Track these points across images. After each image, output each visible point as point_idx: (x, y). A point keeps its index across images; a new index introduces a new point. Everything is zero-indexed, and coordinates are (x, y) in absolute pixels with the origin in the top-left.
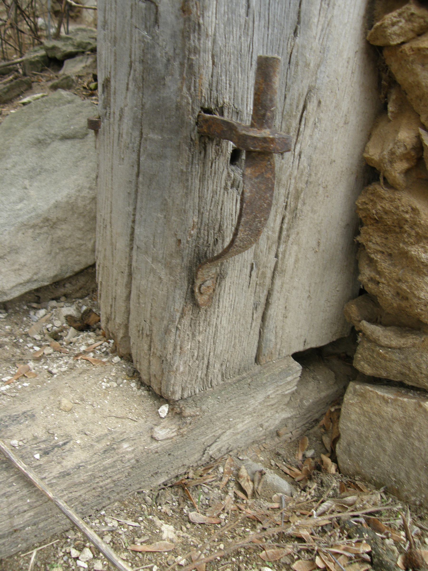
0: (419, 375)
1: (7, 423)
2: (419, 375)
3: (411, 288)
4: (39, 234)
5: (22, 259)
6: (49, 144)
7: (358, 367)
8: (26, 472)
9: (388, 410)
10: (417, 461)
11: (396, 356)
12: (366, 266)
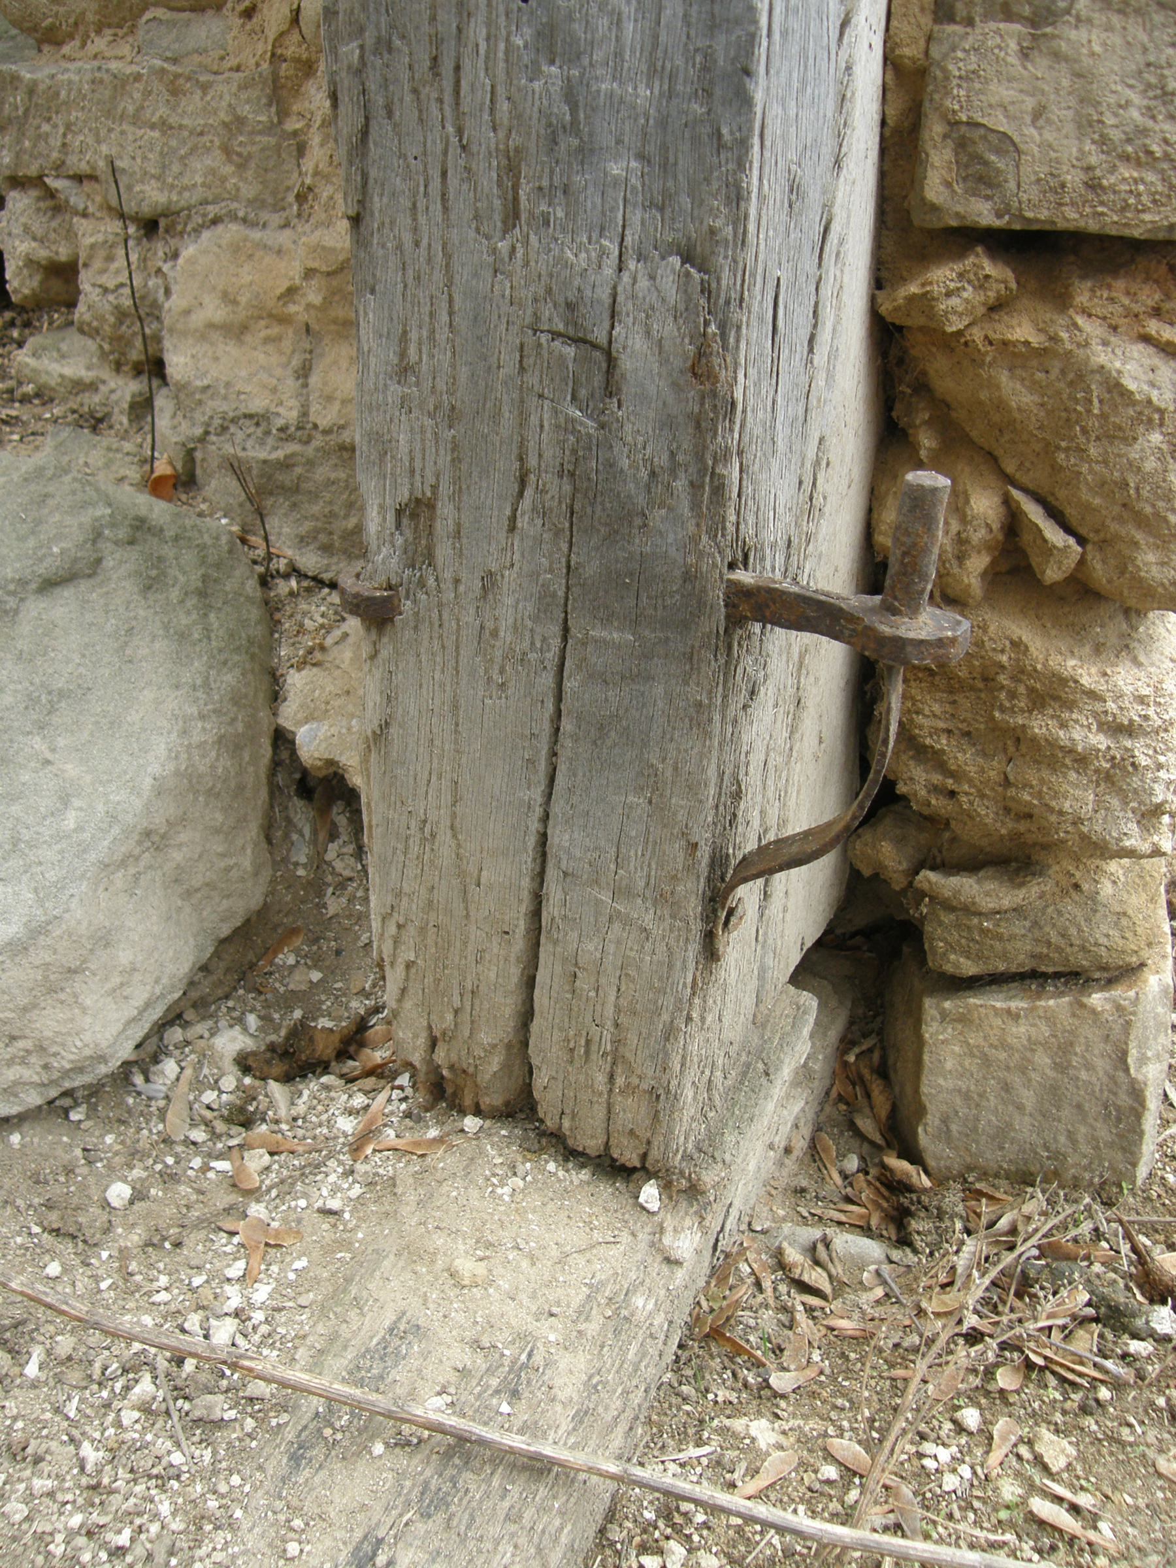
0: (1068, 950)
1: (375, 1371)
2: (1068, 950)
3: (1040, 795)
4: (137, 877)
5: (125, 957)
6: (16, 612)
7: (949, 968)
8: (532, 1449)
9: (1020, 1031)
10: (1087, 1106)
11: (1019, 927)
12: (912, 763)
